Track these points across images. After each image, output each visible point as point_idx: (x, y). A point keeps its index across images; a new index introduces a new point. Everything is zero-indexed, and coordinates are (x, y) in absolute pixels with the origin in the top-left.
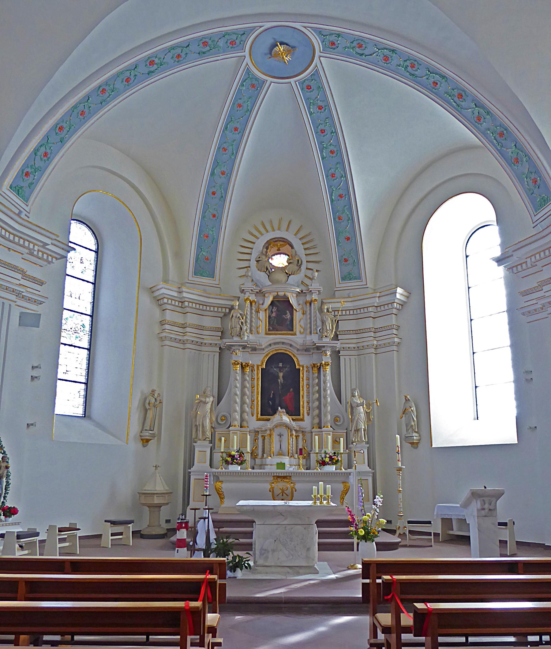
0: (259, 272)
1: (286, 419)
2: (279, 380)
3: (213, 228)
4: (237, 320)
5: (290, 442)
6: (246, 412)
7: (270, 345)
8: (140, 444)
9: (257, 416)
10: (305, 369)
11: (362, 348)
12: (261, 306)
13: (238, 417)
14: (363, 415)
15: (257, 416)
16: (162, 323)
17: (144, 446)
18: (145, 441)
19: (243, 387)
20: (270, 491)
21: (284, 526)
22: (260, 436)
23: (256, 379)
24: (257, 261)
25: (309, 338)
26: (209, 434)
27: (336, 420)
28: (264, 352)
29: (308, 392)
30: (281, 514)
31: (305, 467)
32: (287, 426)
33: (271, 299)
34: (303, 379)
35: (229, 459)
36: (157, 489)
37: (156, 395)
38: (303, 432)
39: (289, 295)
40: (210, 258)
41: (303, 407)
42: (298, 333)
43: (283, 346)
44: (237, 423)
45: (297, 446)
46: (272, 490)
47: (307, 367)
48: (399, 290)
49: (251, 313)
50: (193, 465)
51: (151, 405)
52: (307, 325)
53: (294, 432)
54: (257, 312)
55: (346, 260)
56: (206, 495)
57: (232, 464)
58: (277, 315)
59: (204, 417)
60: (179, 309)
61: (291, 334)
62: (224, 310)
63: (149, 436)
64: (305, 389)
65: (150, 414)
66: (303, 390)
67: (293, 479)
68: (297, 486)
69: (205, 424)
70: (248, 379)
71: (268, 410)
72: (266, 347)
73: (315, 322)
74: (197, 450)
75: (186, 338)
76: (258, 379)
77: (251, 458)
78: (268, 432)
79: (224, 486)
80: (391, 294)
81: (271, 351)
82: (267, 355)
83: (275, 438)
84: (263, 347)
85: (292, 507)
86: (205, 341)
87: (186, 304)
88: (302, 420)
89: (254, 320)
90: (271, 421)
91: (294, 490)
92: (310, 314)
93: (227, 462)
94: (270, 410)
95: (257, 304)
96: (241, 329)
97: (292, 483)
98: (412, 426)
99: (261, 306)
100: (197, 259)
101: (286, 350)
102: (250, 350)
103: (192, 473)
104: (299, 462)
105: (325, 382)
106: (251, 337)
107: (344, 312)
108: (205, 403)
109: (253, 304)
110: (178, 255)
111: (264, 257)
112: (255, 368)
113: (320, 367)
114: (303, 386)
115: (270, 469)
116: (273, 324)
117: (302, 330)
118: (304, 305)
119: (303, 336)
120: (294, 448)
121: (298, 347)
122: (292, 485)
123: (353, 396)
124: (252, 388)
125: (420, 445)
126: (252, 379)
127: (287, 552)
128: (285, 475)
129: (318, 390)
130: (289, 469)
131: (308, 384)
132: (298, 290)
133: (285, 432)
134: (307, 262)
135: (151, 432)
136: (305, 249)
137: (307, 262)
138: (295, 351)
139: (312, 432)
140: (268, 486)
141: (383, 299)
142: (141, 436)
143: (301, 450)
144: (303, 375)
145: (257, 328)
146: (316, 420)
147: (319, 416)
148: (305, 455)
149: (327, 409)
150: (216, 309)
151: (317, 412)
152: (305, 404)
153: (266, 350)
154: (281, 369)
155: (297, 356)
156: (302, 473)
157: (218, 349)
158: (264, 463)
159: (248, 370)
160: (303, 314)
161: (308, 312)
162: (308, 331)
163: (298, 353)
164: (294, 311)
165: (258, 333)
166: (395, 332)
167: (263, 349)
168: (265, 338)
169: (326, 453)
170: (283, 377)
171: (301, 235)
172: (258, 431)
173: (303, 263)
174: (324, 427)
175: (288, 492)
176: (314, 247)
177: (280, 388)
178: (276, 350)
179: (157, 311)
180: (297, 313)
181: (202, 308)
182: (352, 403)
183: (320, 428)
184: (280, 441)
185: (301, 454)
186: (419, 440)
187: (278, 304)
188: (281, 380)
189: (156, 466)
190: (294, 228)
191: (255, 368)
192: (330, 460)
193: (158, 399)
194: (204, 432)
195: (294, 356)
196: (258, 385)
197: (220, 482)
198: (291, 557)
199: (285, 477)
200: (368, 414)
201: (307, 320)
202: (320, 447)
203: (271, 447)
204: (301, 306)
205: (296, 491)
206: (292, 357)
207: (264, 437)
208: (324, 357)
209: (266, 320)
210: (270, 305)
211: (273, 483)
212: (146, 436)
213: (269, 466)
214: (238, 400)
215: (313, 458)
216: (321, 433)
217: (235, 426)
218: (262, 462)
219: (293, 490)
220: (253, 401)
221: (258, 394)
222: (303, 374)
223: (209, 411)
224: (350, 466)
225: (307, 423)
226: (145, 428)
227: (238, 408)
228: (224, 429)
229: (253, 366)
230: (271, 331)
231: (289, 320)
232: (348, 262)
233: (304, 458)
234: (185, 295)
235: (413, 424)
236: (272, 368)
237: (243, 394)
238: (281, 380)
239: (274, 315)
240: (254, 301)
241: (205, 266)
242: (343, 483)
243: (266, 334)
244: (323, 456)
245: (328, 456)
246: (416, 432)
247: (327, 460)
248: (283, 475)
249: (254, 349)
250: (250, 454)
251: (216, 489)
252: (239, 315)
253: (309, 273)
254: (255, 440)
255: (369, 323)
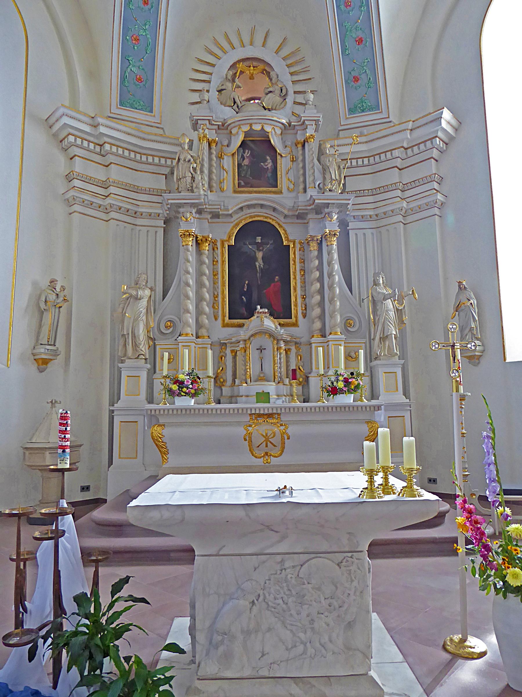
0: (223, 106)
1: (270, 323)
2: (257, 264)
3: (145, 25)
4: (186, 164)
5: (277, 358)
6: (205, 314)
7: (241, 209)
8: (34, 367)
9: (224, 321)
10: (298, 246)
11: (384, 216)
12: (225, 148)
13: (191, 321)
14: (392, 314)
15: (224, 321)
16: (69, 178)
17: (41, 371)
18: (40, 362)
19: (200, 274)
20: (245, 440)
21: (279, 558)
22: (228, 351)
23: (220, 262)
24: (220, 91)
25: (302, 198)
26: (144, 348)
27: (347, 324)
28: (232, 220)
29: (304, 282)
30: (269, 528)
31: (302, 399)
32: (271, 335)
33: (241, 137)
34: (294, 261)
35: (175, 387)
36: (51, 441)
37: (58, 289)
38: (296, 343)
39: (268, 129)
40: (144, 77)
41: (296, 305)
42: (284, 190)
43: (262, 210)
44: (191, 330)
45: (288, 366)
46: (249, 438)
47: (300, 243)
48: (447, 114)
49: (210, 160)
50: (119, 399)
51: (48, 303)
52: (299, 178)
53: (282, 344)
54: (220, 157)
55: (356, 79)
56: (63, 471)
57: (179, 395)
58: (251, 162)
59: (136, 320)
60: (98, 158)
61: (275, 193)
62: (169, 162)
63: (46, 354)
64: (298, 277)
65: (48, 318)
66: (295, 278)
67: (283, 418)
68: (291, 430)
69: (136, 331)
70: (207, 261)
71: (241, 308)
72: (236, 212)
73: (312, 171)
74: (124, 374)
75: (109, 201)
76: (223, 262)
77: (215, 385)
78: (241, 345)
79: (166, 432)
80: (432, 121)
81: (244, 218)
82: (237, 225)
83: (253, 354)
84: (230, 212)
85: (304, 510)
86: (141, 210)
87: (107, 147)
88: (295, 325)
89: (214, 171)
90: (245, 327)
91: (286, 438)
92: (304, 160)
93: (171, 392)
94: (243, 311)
95: (219, 145)
96: (193, 178)
97: (281, 425)
98: (471, 329)
99: (225, 148)
100: (123, 79)
101: (266, 217)
102: (209, 216)
103: (115, 413)
104: (291, 390)
105: (329, 264)
106: (212, 196)
107: (354, 161)
108: (137, 299)
109: (213, 145)
110: (93, 75)
111: (229, 85)
112: (219, 244)
113: (321, 241)
114: (295, 273)
115: (246, 403)
116: (245, 176)
117: (292, 186)
118: (294, 147)
119: (293, 195)
120: (283, 369)
121: (286, 212)
122: (282, 428)
123: (376, 283)
124: (214, 275)
125: (483, 361)
126: (214, 262)
127: (286, 635)
128: (270, 412)
129: (319, 277)
130: (276, 403)
131: (303, 270)
132: (284, 121)
133: (268, 343)
134: (295, 92)
135: (48, 347)
136: (292, 74)
137: (295, 92)
138: (282, 219)
139: (311, 344)
140: (241, 431)
141: (418, 133)
142: (34, 355)
143: (294, 371)
144: (295, 255)
145: (221, 183)
146: (318, 325)
147: (322, 317)
148: (301, 380)
149: (335, 305)
150: (156, 160)
151: (317, 311)
152: (299, 300)
153: (235, 217)
154: (259, 246)
155: (283, 225)
156: (298, 408)
157: (161, 223)
158: (236, 394)
159: (206, 247)
160: (293, 161)
161: (301, 158)
162: (302, 187)
163: (288, 220)
164: (279, 157)
165: (222, 190)
166: (436, 186)
167: (231, 215)
168: (234, 198)
169: (337, 375)
170: (263, 258)
171: (285, 52)
172: (226, 344)
173: (289, 93)
174: (330, 334)
175: (276, 440)
176: (305, 71)
177: (260, 276)
178: (251, 217)
179: (61, 159)
180: (283, 159)
181: (288, 601)
182: (374, 294)
183: (324, 336)
184: (262, 359)
185: (294, 378)
186: (483, 352)
187: (252, 145)
188: (259, 263)
189: (52, 402)
190: (274, 42)
191: (219, 244)
192: (345, 386)
193: (62, 295)
194: (135, 346)
195: (281, 226)
196: (223, 271)
197: (159, 426)
198: (301, 648)
199: (270, 415)
200: (399, 312)
201: (298, 171)
202: (327, 367)
203: (246, 369)
204: (288, 149)
205: (288, 438)
206: (277, 227)
207: (235, 354)
208: (327, 223)
209: (234, 170)
210: (240, 146)
211: (250, 426)
212: (41, 353)
213: (244, 398)
214: (191, 294)
215: (315, 384)
216: (326, 344)
217: (187, 335)
218: (233, 391)
219: (284, 437)
220: (215, 297)
221: (223, 285)
222: (294, 253)
223: (144, 311)
224: (373, 396)
225: (300, 331)
226: (40, 342)
227: (191, 307)
228: (171, 341)
229: (214, 243)
230: (243, 187)
231: (270, 170)
232: (360, 82)
233: (300, 384)
234: (102, 129)
235: (473, 325)
236: (245, 244)
237: (200, 285)
238: (259, 263)
239: (246, 162)
240: (214, 141)
241: (137, 90)
242: (367, 422)
243: (235, 192)
244: (333, 379)
245: (341, 378)
246: (478, 339)
247: (341, 385)
248: (266, 412)
249: (216, 216)
250: (213, 380)
251: (152, 437)
252: (189, 157)
253: (300, 99)
254: (219, 359)
255: (394, 176)
